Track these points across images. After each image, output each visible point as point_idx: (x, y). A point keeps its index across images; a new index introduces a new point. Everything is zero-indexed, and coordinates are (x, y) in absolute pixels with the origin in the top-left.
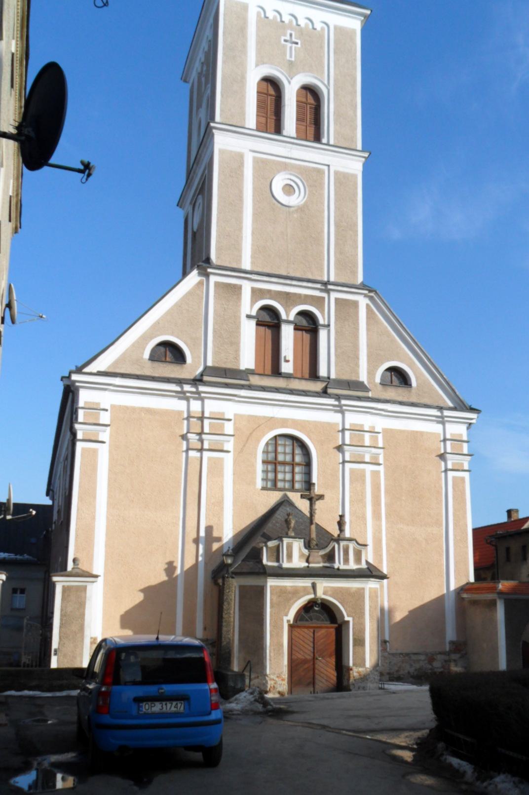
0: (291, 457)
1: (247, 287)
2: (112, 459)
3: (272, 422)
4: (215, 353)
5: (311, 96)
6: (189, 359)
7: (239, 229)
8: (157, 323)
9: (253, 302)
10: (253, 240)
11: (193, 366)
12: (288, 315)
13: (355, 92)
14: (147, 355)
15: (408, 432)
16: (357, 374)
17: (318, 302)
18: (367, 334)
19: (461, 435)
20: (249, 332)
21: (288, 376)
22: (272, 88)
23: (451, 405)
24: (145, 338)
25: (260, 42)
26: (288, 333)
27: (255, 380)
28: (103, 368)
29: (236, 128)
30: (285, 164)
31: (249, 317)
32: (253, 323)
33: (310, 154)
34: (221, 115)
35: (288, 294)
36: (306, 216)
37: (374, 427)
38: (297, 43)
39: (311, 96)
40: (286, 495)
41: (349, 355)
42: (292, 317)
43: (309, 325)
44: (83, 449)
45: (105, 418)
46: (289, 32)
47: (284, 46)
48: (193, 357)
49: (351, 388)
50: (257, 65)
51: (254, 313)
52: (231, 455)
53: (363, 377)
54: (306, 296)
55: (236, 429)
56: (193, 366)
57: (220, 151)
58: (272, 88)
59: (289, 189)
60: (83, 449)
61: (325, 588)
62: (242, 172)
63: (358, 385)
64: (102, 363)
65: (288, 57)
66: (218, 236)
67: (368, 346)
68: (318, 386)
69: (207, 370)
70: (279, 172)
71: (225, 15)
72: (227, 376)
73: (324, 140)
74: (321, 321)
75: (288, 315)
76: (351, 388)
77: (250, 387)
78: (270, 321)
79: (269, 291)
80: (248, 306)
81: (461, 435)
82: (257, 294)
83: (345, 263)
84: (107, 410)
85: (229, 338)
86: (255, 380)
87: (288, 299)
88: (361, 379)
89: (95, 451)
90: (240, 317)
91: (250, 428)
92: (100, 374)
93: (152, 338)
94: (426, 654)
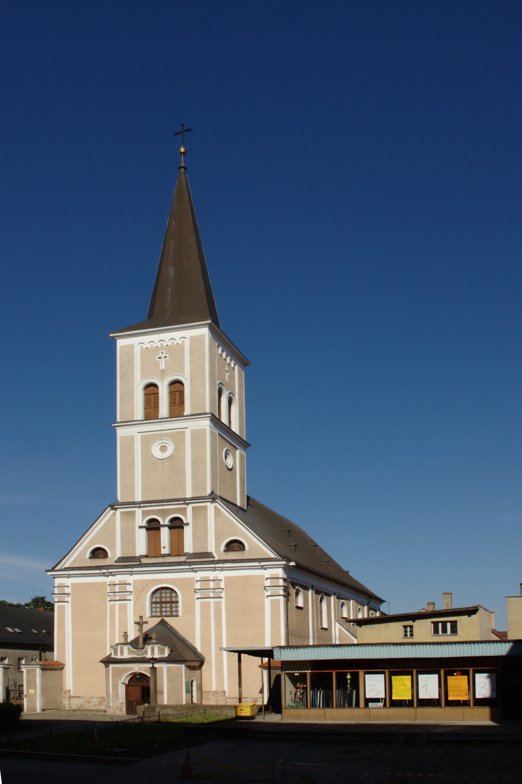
0: (165, 599)
1: (139, 512)
2: (73, 610)
3: (155, 581)
4: (122, 550)
5: (176, 386)
6: (110, 555)
7: (133, 481)
8: (92, 539)
9: (143, 519)
10: (142, 484)
11: (111, 560)
12: (164, 522)
13: (205, 376)
14: (88, 555)
15: (241, 576)
16: (207, 548)
17: (184, 511)
18: (215, 524)
19: (278, 574)
20: (141, 536)
21: (164, 556)
22: (151, 389)
23: (272, 555)
24: (86, 548)
25: (143, 365)
26: (165, 533)
27: (144, 561)
28: (67, 566)
29: (129, 423)
30: (162, 434)
31: (140, 527)
32: (144, 530)
33: (177, 424)
34: (120, 417)
35: (163, 510)
36: (175, 462)
37: (217, 577)
38: (159, 358)
39: (176, 386)
40: (163, 620)
41: (200, 536)
42: (167, 522)
43: (177, 525)
44: (58, 606)
45: (67, 590)
46: (160, 352)
47: (158, 362)
48: (112, 554)
49: (202, 558)
50: (141, 380)
51: (144, 524)
52: (132, 603)
53: (211, 548)
54: (175, 509)
55: (134, 588)
56: (111, 560)
57: (121, 438)
58: (151, 389)
59: (163, 449)
60: (58, 606)
61: (137, 668)
62: (133, 446)
63: (209, 555)
64: (68, 562)
65: (161, 369)
66: (121, 486)
67: (215, 530)
68: (182, 559)
69: (121, 559)
70: (150, 450)
71: (120, 356)
72: (129, 562)
73: (187, 412)
74: (185, 522)
75: (164, 522)
76: (202, 558)
77: (141, 565)
78: (153, 526)
79: (152, 511)
80: (140, 519)
81: (278, 574)
82: (145, 514)
83: (197, 483)
84: (68, 587)
85: (129, 538)
86: (144, 561)
87: (164, 513)
88: (209, 551)
89: (64, 606)
90: (135, 529)
91: (142, 586)
92: (66, 569)
93: (90, 547)
94: (252, 698)
